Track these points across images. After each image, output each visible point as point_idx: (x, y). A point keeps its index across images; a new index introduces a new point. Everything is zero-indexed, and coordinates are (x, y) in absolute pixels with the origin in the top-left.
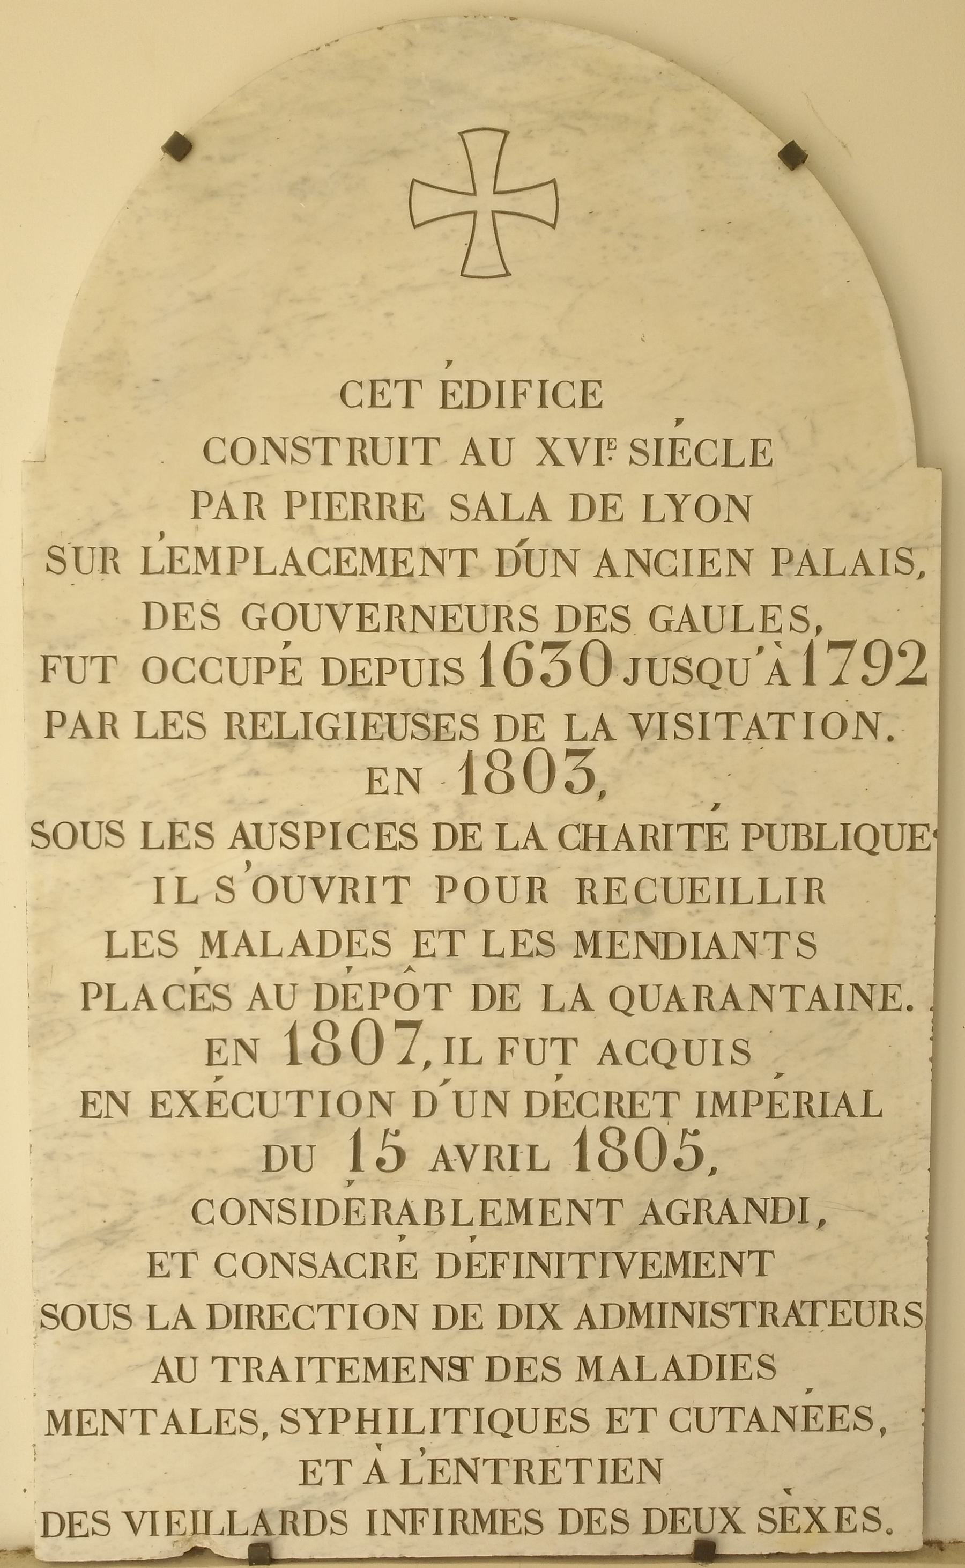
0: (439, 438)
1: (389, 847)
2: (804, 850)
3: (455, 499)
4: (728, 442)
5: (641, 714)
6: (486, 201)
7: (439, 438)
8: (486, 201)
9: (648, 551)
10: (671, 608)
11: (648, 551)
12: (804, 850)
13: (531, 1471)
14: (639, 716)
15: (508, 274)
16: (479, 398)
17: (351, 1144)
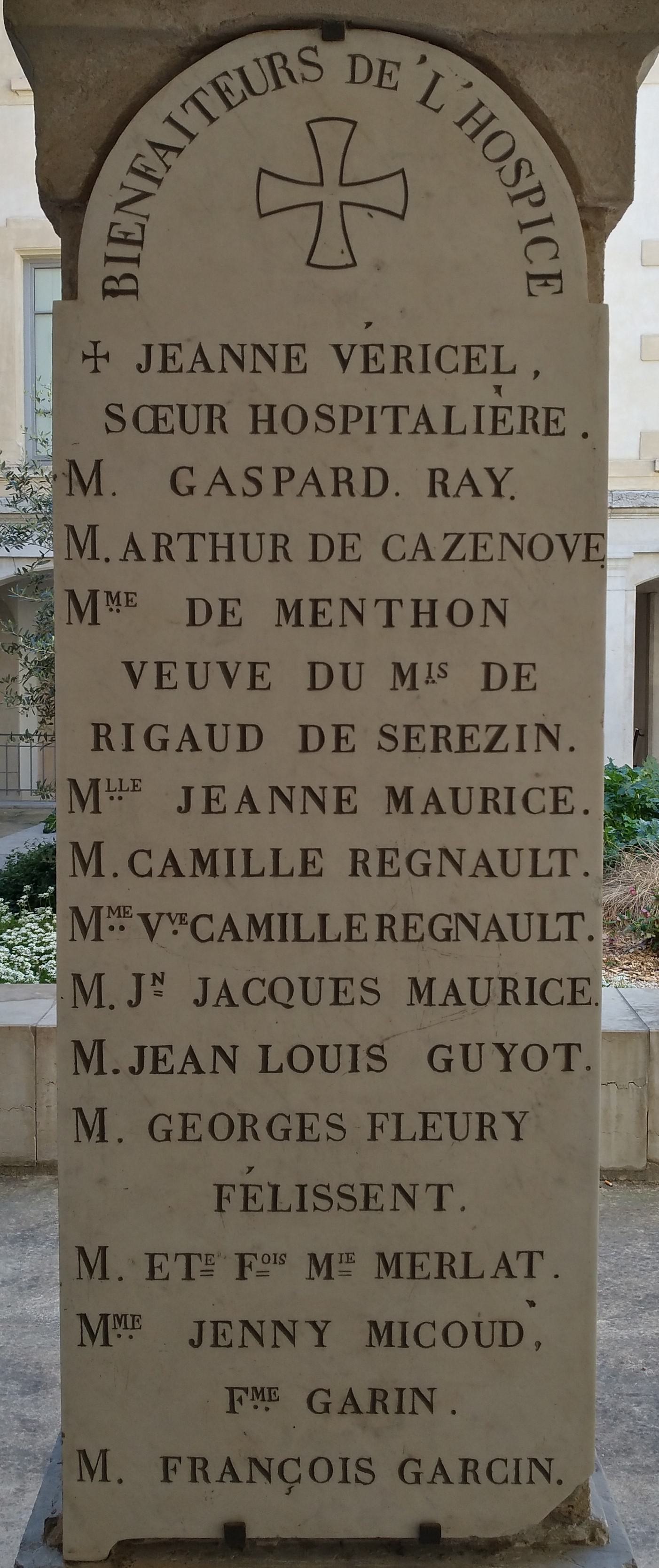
6: (331, 195)
8: (331, 195)
13: (449, 738)
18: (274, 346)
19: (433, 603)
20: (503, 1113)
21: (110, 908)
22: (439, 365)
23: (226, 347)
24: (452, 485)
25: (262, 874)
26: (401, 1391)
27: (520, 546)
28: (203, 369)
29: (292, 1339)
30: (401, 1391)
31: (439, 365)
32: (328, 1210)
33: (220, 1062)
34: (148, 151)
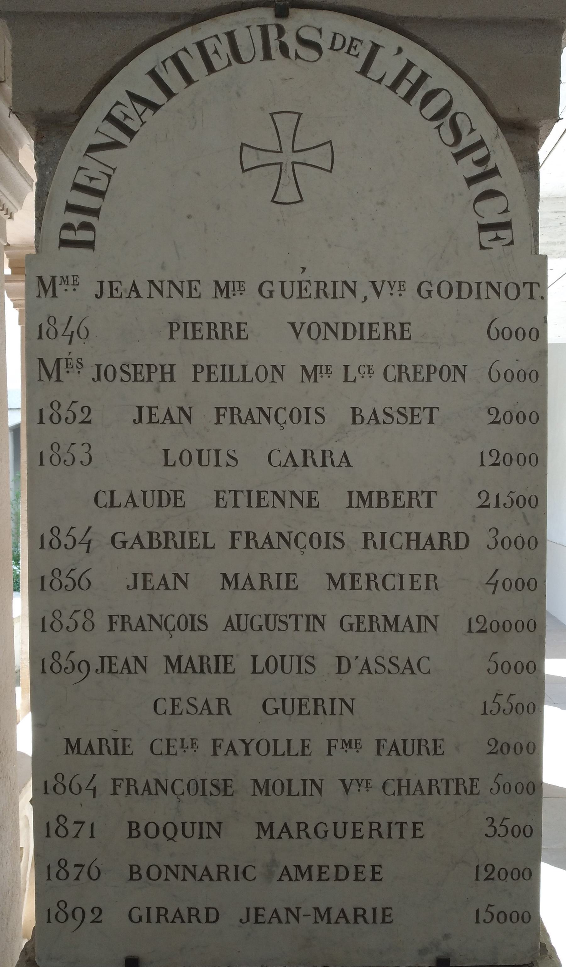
0: (234, 673)
1: (86, 416)
2: (156, 548)
3: (81, 367)
4: (112, 492)
5: (153, 114)
6: (287, 157)
7: (234, 673)
8: (287, 157)
9: (161, 616)
10: (124, 533)
11: (161, 616)
12: (156, 548)
13: (228, 705)
14: (153, 112)
15: (508, 496)
16: (342, 875)
17: (38, 329)
18: (162, 282)
19: (418, 534)
20: (240, 739)
21: (62, 277)
22: (268, 743)
23: (151, 282)
24: (170, 917)
25: (120, 506)
26: (335, 283)
27: (160, 623)
28: (233, 754)
29: (219, 834)
30: (335, 283)
31: (268, 743)
32: (489, 740)
33: (291, 916)
34: (126, 100)
